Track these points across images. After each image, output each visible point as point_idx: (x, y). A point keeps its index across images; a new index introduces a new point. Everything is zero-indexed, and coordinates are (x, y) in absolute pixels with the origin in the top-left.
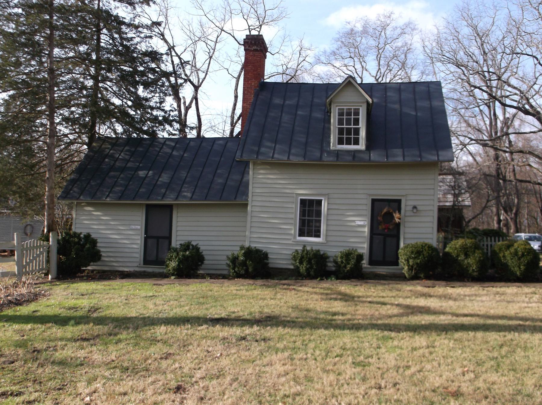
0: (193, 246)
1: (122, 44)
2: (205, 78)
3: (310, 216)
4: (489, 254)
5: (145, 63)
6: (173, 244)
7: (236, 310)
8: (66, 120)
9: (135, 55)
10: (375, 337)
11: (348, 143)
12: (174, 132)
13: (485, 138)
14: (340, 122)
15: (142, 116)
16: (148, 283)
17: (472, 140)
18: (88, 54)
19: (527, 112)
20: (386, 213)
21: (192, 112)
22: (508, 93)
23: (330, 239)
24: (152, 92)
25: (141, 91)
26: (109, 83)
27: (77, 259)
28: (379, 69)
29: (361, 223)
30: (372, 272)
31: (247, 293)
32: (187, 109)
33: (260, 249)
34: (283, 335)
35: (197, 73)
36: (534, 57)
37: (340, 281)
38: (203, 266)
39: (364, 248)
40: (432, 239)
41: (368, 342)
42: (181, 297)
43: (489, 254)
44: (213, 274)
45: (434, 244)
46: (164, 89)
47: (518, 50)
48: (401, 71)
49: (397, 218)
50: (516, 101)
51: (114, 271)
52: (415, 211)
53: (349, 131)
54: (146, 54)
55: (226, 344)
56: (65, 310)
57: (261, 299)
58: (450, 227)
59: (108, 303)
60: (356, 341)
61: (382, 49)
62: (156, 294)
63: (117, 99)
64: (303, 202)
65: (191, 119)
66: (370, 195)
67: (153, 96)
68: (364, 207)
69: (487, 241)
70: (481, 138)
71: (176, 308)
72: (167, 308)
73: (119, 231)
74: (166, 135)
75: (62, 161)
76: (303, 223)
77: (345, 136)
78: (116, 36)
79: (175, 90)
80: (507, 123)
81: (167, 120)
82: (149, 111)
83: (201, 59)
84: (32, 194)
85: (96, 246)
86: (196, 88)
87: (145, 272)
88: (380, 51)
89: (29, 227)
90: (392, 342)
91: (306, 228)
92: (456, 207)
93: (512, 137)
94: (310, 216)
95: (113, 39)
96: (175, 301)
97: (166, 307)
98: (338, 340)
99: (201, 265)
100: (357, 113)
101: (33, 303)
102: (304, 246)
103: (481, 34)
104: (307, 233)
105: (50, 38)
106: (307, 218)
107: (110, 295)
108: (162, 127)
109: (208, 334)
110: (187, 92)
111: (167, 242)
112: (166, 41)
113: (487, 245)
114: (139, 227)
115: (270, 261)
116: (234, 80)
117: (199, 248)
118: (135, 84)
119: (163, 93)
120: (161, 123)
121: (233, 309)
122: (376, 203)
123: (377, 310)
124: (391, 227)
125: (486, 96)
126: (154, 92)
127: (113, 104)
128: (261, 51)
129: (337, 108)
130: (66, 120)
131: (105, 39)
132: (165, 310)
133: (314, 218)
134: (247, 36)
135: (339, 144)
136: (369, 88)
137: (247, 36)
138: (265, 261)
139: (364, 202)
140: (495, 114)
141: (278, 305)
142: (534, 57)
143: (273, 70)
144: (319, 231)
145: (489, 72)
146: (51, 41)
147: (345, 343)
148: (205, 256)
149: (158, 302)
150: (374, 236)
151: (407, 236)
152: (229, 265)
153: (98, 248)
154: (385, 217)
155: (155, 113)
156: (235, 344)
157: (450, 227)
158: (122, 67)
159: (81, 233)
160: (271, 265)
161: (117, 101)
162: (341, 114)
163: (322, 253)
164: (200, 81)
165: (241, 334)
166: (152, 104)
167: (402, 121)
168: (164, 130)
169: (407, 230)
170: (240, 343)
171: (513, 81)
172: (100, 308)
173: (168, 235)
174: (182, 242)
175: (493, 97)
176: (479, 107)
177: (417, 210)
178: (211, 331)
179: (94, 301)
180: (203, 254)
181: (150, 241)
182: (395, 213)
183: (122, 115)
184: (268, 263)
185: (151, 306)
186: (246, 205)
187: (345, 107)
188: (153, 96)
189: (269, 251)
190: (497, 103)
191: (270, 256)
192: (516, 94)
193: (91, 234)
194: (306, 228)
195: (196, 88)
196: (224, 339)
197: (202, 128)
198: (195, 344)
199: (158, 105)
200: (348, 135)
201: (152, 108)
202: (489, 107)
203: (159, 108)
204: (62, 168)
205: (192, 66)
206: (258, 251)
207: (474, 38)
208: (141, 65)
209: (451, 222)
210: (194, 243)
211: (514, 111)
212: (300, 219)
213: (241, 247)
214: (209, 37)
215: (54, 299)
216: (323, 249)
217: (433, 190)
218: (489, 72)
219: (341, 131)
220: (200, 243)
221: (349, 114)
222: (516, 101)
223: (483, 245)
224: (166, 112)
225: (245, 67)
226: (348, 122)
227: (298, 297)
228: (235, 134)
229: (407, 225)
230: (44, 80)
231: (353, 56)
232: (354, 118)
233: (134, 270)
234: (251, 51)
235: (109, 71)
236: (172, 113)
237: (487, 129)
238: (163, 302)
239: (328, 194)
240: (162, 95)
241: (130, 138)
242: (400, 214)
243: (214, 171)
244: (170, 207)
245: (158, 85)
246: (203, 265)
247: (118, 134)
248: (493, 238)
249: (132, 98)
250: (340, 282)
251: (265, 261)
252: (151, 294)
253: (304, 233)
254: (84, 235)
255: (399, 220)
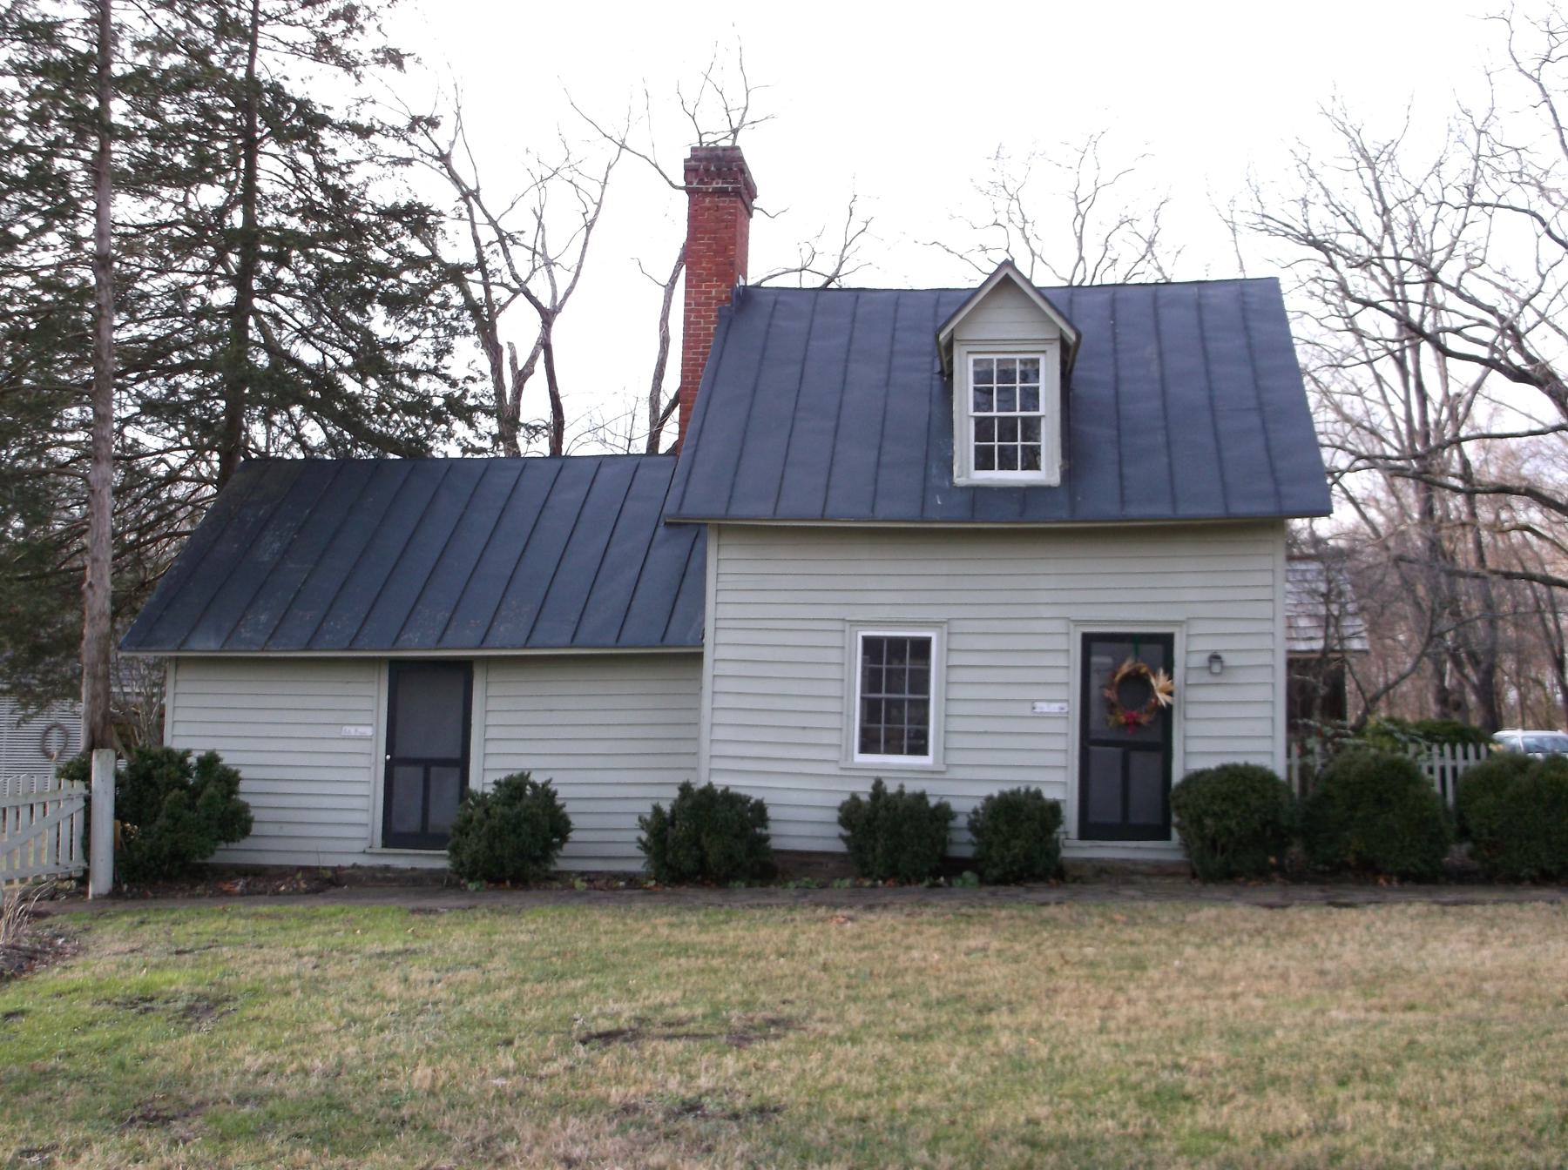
0: (534, 785)
1: (323, 186)
2: (572, 287)
3: (895, 691)
4: (1450, 798)
5: (390, 239)
6: (475, 783)
7: (667, 1000)
8: (150, 407)
9: (362, 217)
10: (1132, 1094)
11: (1008, 463)
12: (478, 444)
13: (1390, 452)
14: (983, 398)
15: (385, 396)
16: (393, 907)
17: (1360, 457)
18: (221, 212)
19: (1518, 376)
20: (1127, 677)
21: (536, 387)
22: (1458, 322)
23: (955, 758)
24: (412, 322)
25: (380, 323)
26: (279, 298)
27: (181, 837)
28: (1081, 258)
29: (1054, 708)
30: (1089, 860)
31: (704, 938)
32: (521, 377)
33: (743, 792)
34: (822, 1092)
35: (550, 271)
36: (1534, 214)
37: (992, 888)
38: (567, 849)
39: (1057, 779)
40: (1272, 753)
41: (1113, 1116)
42: (492, 954)
43: (1450, 798)
44: (599, 874)
45: (1280, 771)
46: (447, 314)
47: (1484, 194)
48: (1144, 262)
49: (1162, 691)
50: (1485, 344)
51: (291, 867)
52: (1216, 668)
53: (1008, 429)
54: (393, 213)
55: (632, 1131)
56: (110, 1008)
57: (748, 956)
58: (1317, 714)
59: (253, 980)
60: (1070, 1112)
61: (1089, 201)
62: (416, 945)
63: (309, 347)
64: (871, 646)
65: (535, 407)
66: (1078, 622)
67: (415, 338)
68: (1061, 660)
69: (1454, 757)
70: (1378, 451)
71: (472, 994)
72: (444, 995)
73: (305, 749)
74: (454, 452)
75: (140, 535)
76: (871, 710)
77: (996, 443)
78: (305, 160)
79: (485, 323)
80: (1457, 407)
81: (458, 408)
82: (406, 381)
83: (561, 239)
84: (50, 636)
85: (237, 793)
86: (548, 316)
87: (387, 868)
88: (1083, 207)
89: (55, 733)
90: (1193, 1112)
91: (883, 726)
92: (1331, 655)
93: (1469, 448)
94: (895, 691)
95: (297, 168)
96: (473, 970)
97: (441, 991)
98: (1009, 1105)
99: (560, 846)
100: (1030, 372)
101: (15, 984)
102: (878, 784)
103: (1372, 153)
104: (887, 742)
105: (99, 169)
106: (883, 695)
107: (265, 950)
108: (443, 427)
109: (572, 1092)
110: (517, 327)
111: (454, 774)
112: (456, 180)
113: (1443, 770)
114: (368, 731)
115: (773, 828)
116: (661, 292)
117: (555, 793)
118: (360, 301)
119: (445, 327)
120: (438, 417)
121: (658, 997)
122: (1096, 646)
123: (1120, 989)
124: (1144, 719)
125: (1389, 328)
126: (421, 324)
127: (297, 362)
128: (737, 193)
129: (972, 358)
130: (150, 407)
131: (271, 166)
132: (435, 1004)
133: (907, 696)
134: (693, 149)
135: (978, 467)
136: (1068, 300)
137: (693, 149)
138: (758, 830)
139: (1061, 642)
140: (1420, 386)
141: (802, 977)
142: (1534, 214)
143: (773, 255)
144: (923, 735)
145: (1398, 258)
146: (104, 177)
147: (1032, 1122)
148: (573, 819)
149: (415, 975)
150: (1093, 748)
151: (1194, 746)
152: (644, 846)
153: (242, 798)
154: (1126, 686)
155: (422, 384)
156: (663, 1129)
157: (1317, 714)
158: (320, 251)
159: (188, 753)
160: (775, 844)
161: (309, 355)
162: (982, 376)
163: (933, 802)
164: (560, 297)
165: (682, 1091)
166: (410, 358)
167: (1159, 409)
168: (448, 435)
169: (1194, 728)
170: (678, 1127)
171: (1471, 285)
172: (227, 1000)
173: (457, 754)
174: (502, 776)
175: (1412, 332)
176: (1370, 362)
177: (1223, 667)
178: (582, 1081)
179: (214, 974)
180: (566, 810)
181: (401, 772)
182: (1155, 674)
183: (322, 393)
184: (767, 838)
185: (394, 989)
186: (699, 657)
187: (995, 357)
188: (415, 338)
189: (768, 798)
190: (1426, 348)
191: (771, 813)
192: (1483, 323)
193: (221, 755)
194: (883, 726)
195: (548, 316)
196: (628, 1109)
197: (566, 434)
198: (527, 1132)
199: (432, 362)
200: (1005, 441)
201: (414, 374)
202: (1401, 363)
203: (434, 372)
204: (139, 554)
205: (535, 252)
206: (731, 800)
207: (1353, 165)
208: (380, 244)
209: (1318, 701)
210: (538, 778)
211: (1476, 370)
212: (862, 699)
213: (681, 789)
214: (579, 167)
215: (86, 967)
216: (936, 792)
217: (1270, 604)
218: (1398, 258)
219: (983, 429)
220: (557, 778)
221: (1006, 375)
222: (1485, 344)
223: (1431, 770)
224: (454, 384)
225: (688, 256)
226: (1007, 401)
227: (864, 948)
228: (662, 450)
229: (1193, 712)
230: (84, 292)
231: (1003, 220)
232: (1022, 389)
233: (354, 866)
234: (707, 194)
235: (282, 260)
236: (471, 387)
237: (1397, 427)
238: (433, 975)
239: (948, 622)
240: (441, 333)
241: (345, 461)
242: (1171, 678)
243: (613, 564)
244: (463, 670)
245: (431, 303)
246: (566, 846)
247: (312, 450)
248: (1459, 748)
249: (352, 344)
250: (993, 894)
251: (758, 830)
252: (399, 946)
253: (878, 741)
254: (199, 759)
255: (1168, 699)
